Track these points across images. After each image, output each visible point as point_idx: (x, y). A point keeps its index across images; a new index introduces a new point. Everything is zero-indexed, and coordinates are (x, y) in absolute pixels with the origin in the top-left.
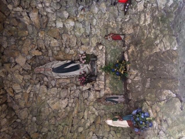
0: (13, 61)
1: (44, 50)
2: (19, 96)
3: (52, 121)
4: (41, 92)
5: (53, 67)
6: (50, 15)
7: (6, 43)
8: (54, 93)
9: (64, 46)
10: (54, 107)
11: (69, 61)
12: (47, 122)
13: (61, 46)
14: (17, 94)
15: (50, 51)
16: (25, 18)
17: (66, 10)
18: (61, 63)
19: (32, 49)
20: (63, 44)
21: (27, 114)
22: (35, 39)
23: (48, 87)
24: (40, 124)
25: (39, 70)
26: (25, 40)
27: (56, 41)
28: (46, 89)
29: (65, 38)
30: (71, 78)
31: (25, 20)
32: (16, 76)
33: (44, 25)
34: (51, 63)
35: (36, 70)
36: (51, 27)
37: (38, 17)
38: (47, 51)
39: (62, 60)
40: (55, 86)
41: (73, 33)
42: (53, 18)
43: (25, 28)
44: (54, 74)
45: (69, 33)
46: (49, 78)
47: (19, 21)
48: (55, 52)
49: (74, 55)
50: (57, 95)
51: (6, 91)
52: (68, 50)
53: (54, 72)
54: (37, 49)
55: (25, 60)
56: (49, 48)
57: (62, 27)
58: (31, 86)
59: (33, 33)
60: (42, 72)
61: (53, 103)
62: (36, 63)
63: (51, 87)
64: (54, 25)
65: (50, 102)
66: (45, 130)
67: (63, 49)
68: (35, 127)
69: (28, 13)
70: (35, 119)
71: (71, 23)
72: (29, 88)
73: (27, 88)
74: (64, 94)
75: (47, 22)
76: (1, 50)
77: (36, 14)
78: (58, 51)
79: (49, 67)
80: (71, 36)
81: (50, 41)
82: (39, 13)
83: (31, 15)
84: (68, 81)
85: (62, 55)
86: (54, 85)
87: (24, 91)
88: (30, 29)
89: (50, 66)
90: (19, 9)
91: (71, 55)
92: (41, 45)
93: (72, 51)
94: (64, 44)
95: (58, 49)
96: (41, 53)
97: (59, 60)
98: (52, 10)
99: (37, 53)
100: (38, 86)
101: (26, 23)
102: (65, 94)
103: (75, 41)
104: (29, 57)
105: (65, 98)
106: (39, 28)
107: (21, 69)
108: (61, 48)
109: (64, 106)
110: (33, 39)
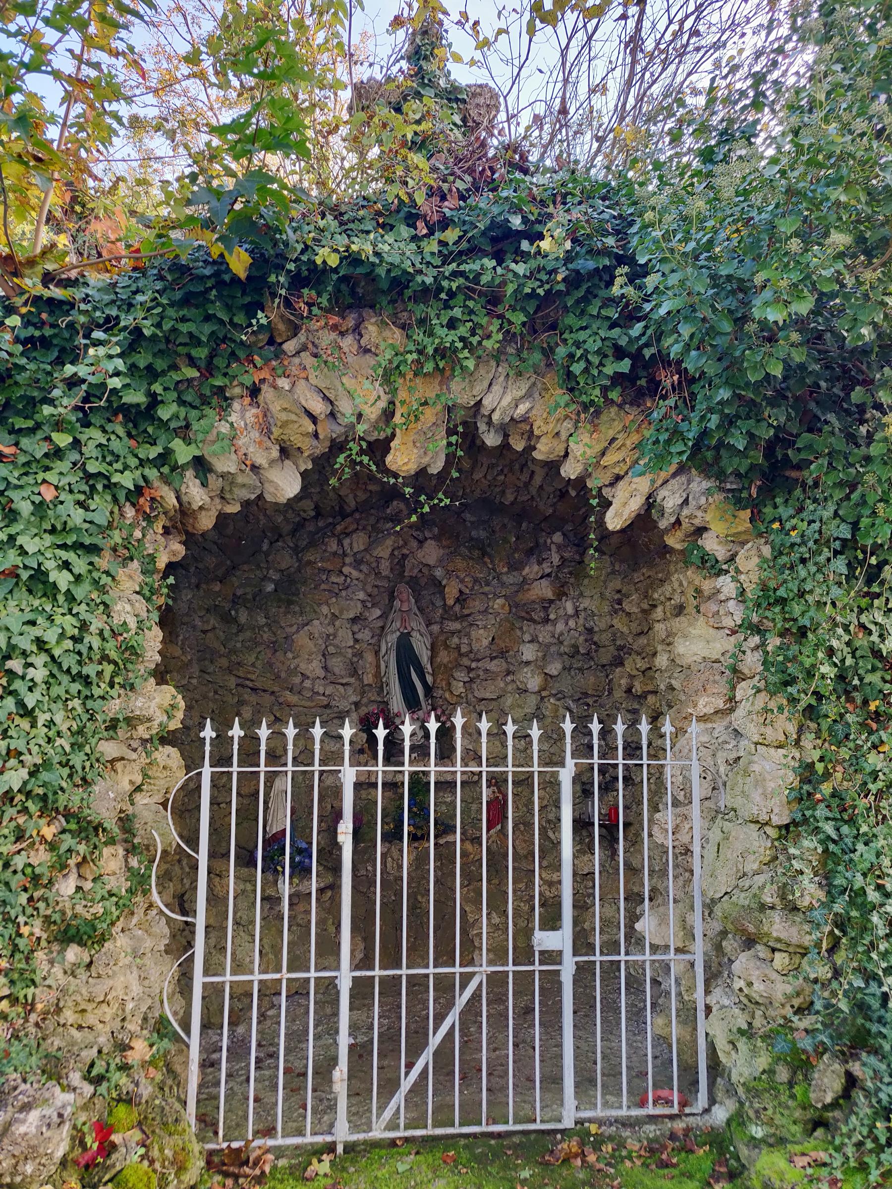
0: (427, 534)
1: (460, 611)
2: (333, 546)
3: (265, 636)
4: (343, 603)
5: (414, 634)
6: (549, 627)
7: (473, 519)
8: (339, 638)
9: (474, 665)
10: (302, 639)
11: (429, 679)
12: (262, 621)
13: (472, 656)
14: (340, 543)
15: (457, 626)
16: (536, 568)
17: (564, 668)
18: (424, 656)
19: (462, 581)
20: (478, 660)
21: (284, 566)
22: (486, 589)
23: (354, 620)
24: (257, 601)
25: (405, 595)
26: (485, 563)
27: (485, 642)
28: (352, 616)
29: (494, 666)
30: (381, 686)
31: (532, 570)
32: (389, 542)
33: (524, 613)
34: (423, 629)
35: (404, 590)
36: (521, 628)
37: (543, 600)
38: (457, 619)
39: (432, 659)
40: (356, 641)
41: (510, 688)
42: (544, 634)
43: (515, 567)
44: (392, 638)
45: (509, 678)
46: (380, 623)
47: (530, 552)
48: (455, 640)
49: (447, 695)
50: (337, 647)
51: (351, 514)
52: (461, 675)
53: (399, 638)
54: (461, 592)
55: (432, 562)
56: (465, 624)
57: (524, 658)
58: (362, 577)
59: (503, 584)
60: (397, 603)
61: (311, 636)
62: (425, 587)
63: (356, 628)
64: (527, 637)
65: (316, 627)
66: (243, 617)
67: (465, 661)
68: (248, 590)
69: (549, 575)
70: (270, 587)
71: (534, 682)
72: (355, 574)
73: (355, 568)
74: (337, 665)
75: (534, 621)
76: (888, 1129)
77: (549, 594)
78: (458, 648)
79: (414, 624)
80: (502, 685)
81: (485, 627)
82: (551, 602)
83: (545, 582)
84: (368, 679)
85: (445, 660)
86: (359, 636)
87: (348, 560)
88: (509, 579)
89: (416, 624)
90: (556, 559)
91: (449, 684)
92: (476, 605)
93: (459, 688)
94: (480, 664)
95: (465, 648)
96: (450, 602)
97: (433, 648)
98: (561, 634)
99: (452, 592)
100: (361, 595)
101: (527, 570)
102: (337, 670)
103: (488, 695)
104: (439, 573)
105: (325, 668)
106: (517, 599)
107: (405, 551)
108: (466, 655)
109: (303, 667)
110: (488, 585)
